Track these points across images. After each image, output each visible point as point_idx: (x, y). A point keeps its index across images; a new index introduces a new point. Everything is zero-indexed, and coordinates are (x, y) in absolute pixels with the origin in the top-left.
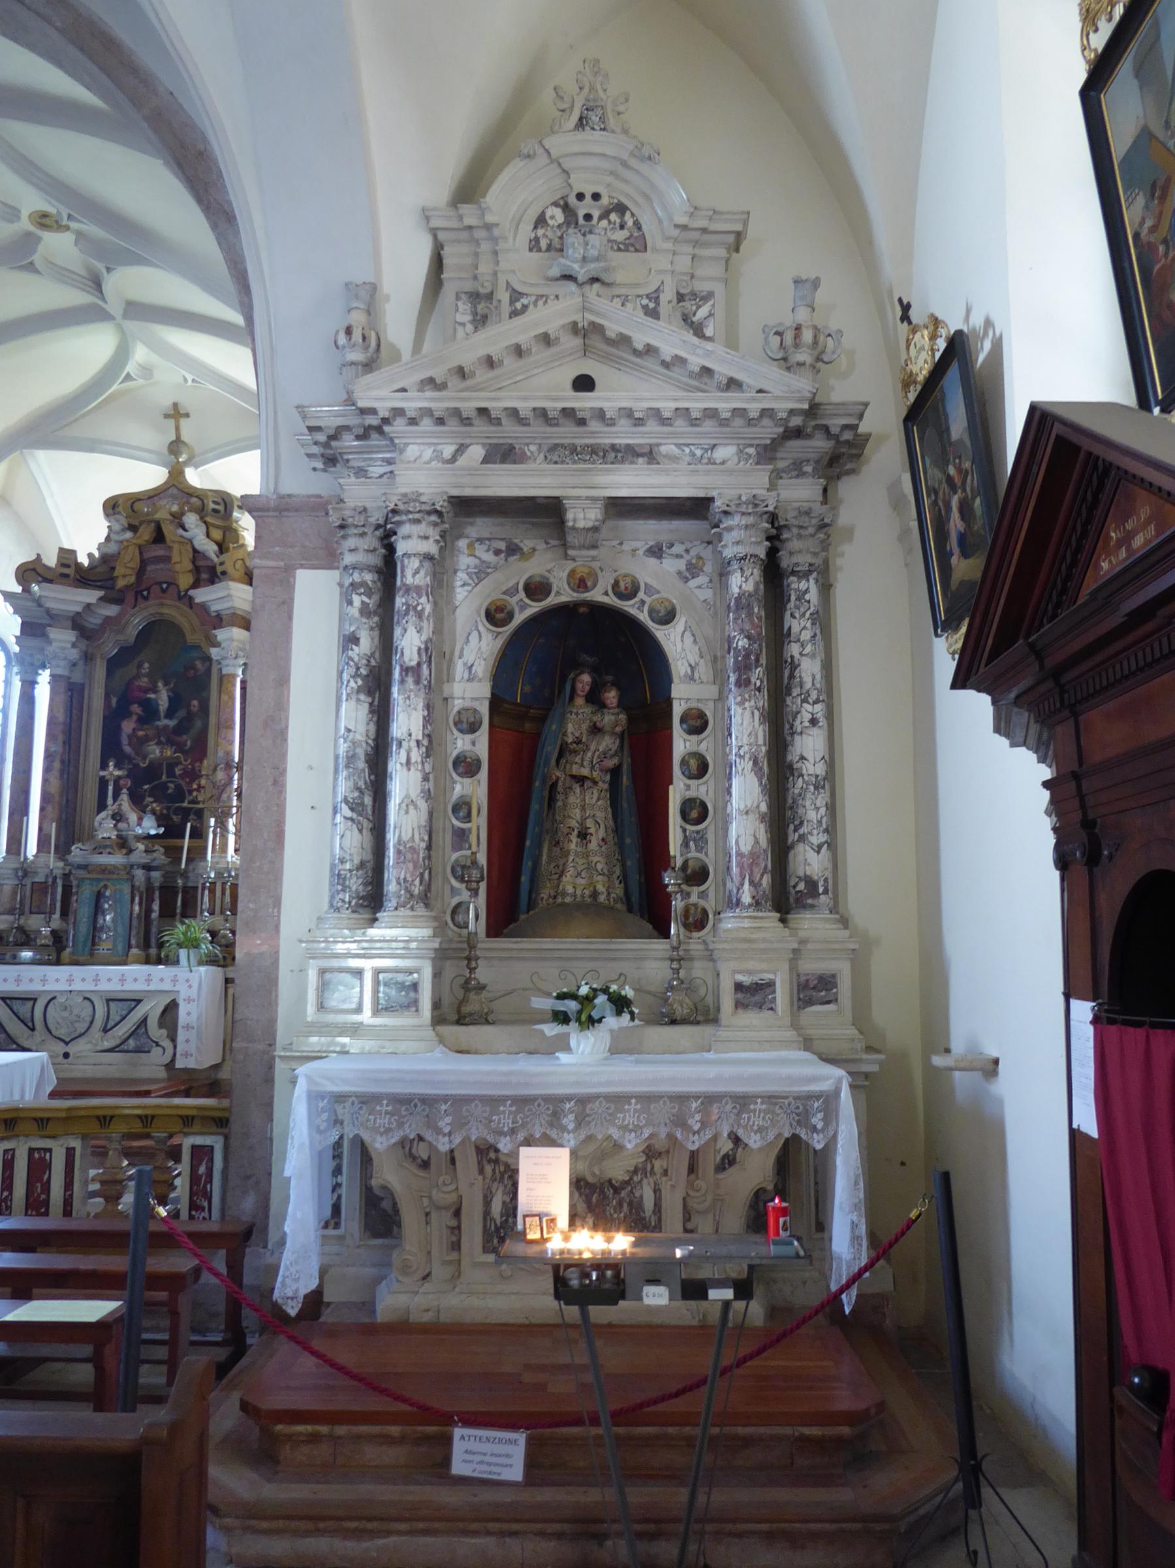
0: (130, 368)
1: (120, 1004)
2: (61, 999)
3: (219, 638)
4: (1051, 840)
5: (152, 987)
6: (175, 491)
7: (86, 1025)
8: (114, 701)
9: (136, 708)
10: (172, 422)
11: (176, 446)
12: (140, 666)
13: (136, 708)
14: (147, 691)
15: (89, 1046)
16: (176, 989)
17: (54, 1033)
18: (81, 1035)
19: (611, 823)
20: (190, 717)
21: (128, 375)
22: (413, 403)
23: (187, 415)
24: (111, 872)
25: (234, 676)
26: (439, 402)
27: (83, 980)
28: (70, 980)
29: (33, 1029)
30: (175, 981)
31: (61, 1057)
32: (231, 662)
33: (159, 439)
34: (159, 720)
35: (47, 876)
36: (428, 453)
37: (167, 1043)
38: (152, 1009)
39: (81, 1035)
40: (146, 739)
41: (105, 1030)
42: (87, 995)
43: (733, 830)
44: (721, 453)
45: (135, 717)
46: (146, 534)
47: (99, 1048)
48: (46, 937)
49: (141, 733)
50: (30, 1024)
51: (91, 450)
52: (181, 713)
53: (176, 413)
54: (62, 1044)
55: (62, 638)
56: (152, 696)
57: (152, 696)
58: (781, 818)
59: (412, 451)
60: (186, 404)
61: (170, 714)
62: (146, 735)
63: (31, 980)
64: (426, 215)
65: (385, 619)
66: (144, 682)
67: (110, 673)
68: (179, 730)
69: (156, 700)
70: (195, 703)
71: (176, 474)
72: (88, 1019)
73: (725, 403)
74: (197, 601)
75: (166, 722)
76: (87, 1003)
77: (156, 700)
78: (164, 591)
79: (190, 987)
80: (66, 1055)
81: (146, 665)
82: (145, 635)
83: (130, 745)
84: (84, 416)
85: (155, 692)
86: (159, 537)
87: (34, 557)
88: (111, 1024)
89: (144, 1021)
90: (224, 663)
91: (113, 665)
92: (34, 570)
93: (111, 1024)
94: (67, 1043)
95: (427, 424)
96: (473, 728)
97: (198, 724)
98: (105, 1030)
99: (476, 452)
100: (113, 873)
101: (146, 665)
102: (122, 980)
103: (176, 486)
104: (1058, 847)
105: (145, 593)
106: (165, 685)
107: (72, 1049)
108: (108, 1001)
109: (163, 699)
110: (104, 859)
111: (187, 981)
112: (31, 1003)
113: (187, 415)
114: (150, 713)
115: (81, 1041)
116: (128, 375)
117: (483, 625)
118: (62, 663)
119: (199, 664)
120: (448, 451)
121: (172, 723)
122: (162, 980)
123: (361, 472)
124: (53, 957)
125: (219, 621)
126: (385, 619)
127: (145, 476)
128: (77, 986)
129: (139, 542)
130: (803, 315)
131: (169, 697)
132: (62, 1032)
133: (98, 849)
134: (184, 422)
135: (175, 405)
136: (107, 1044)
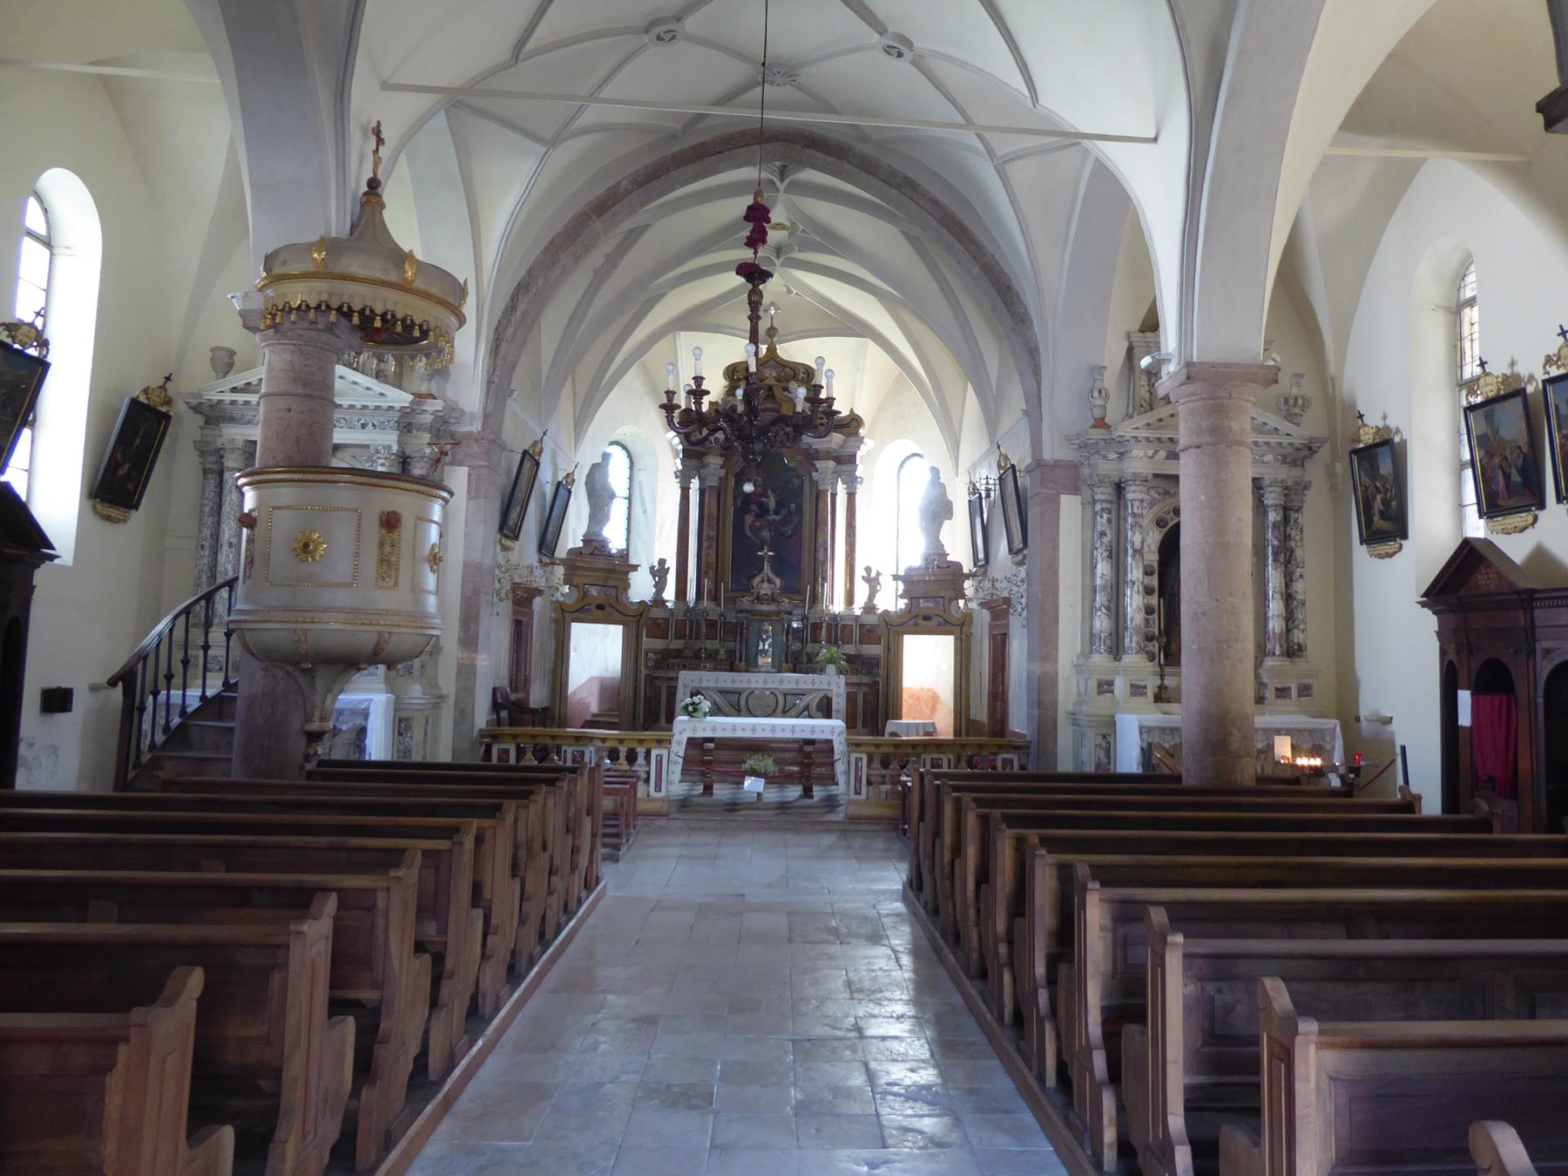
4: (1437, 644)
9: (754, 507)
13: (754, 507)
19: (820, 556)
20: (790, 514)
22: (1142, 434)
26: (1153, 434)
28: (765, 682)
36: (1142, 454)
40: (762, 528)
43: (1271, 626)
44: (1267, 458)
51: (716, 332)
52: (784, 512)
58: (1289, 617)
59: (1135, 452)
61: (776, 512)
64: (1128, 335)
65: (1118, 523)
68: (781, 523)
71: (772, 350)
73: (1273, 440)
95: (1144, 442)
96: (1152, 574)
97: (796, 519)
99: (1162, 454)
103: (772, 359)
104: (1441, 648)
108: (785, 695)
109: (772, 504)
110: (765, 608)
114: (763, 511)
117: (1155, 528)
120: (1150, 453)
121: (778, 518)
123: (1105, 457)
126: (1118, 523)
130: (1295, 391)
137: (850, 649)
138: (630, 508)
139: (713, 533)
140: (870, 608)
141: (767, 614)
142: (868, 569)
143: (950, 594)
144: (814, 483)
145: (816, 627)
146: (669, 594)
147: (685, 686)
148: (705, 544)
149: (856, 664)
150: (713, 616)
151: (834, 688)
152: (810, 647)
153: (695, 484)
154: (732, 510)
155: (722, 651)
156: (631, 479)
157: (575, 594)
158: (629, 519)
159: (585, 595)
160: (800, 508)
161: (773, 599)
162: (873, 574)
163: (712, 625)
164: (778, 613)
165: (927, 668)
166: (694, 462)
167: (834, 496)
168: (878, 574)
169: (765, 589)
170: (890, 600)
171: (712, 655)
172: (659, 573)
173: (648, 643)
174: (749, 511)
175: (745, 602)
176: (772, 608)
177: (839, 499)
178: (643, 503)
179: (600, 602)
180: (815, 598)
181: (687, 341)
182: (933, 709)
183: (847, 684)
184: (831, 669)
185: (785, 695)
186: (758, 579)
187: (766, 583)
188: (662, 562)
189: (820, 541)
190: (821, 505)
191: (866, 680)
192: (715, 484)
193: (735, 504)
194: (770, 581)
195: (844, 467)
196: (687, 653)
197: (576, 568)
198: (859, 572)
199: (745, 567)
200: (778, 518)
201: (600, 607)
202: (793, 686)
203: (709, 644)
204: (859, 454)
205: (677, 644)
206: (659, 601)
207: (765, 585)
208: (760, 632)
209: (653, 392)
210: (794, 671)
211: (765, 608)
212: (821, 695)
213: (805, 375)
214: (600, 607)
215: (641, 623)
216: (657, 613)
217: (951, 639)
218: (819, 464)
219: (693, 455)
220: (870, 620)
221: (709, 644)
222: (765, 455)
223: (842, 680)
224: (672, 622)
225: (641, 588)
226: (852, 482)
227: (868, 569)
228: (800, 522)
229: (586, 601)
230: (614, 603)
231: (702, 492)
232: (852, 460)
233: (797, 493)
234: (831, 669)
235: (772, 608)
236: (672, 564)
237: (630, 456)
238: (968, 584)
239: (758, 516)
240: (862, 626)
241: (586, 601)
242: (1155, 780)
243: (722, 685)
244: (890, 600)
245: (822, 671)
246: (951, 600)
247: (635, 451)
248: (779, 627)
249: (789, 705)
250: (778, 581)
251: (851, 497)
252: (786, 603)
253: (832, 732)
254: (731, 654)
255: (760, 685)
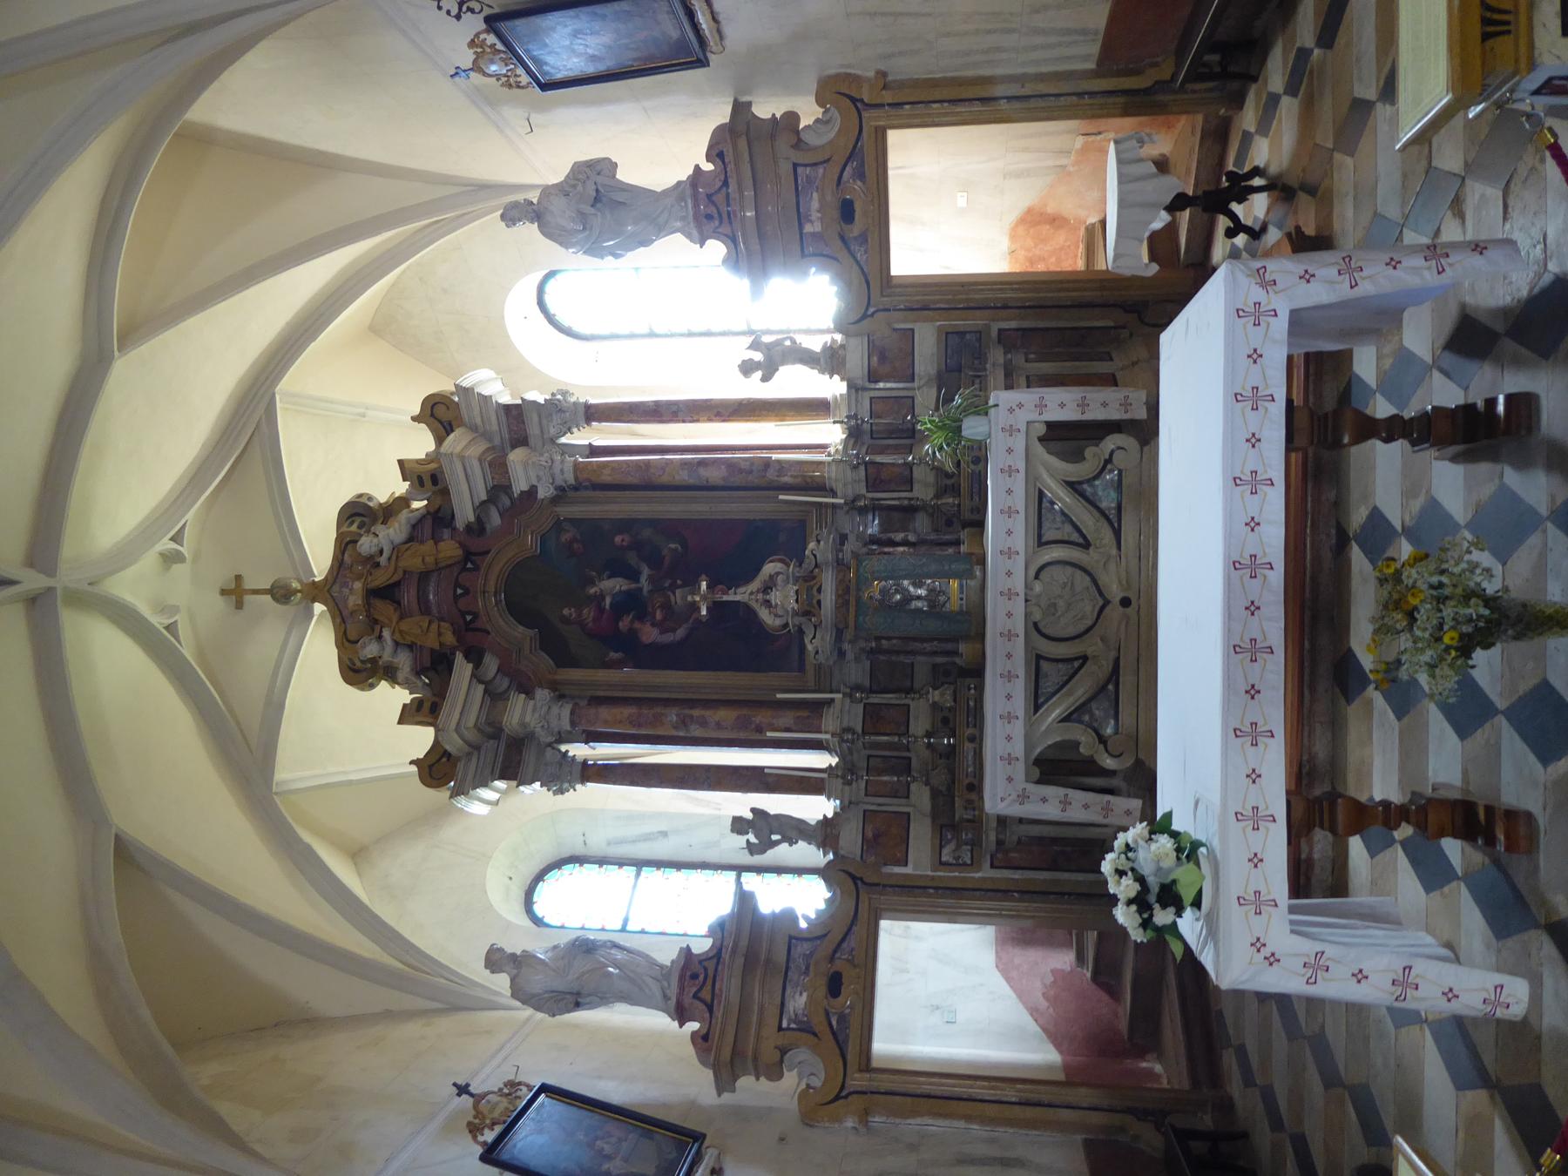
0: (158, 621)
1: (1046, 525)
2: (1037, 616)
3: (525, 487)
5: (1021, 465)
6: (336, 588)
7: (1079, 573)
8: (613, 655)
9: (624, 625)
10: (248, 598)
11: (281, 593)
12: (566, 621)
14: (601, 610)
15: (1112, 567)
16: (1023, 428)
17: (1089, 623)
18: (1095, 582)
21: (167, 628)
23: (238, 578)
24: (847, 590)
25: (576, 465)
27: (1009, 697)
29: (1085, 658)
30: (1011, 431)
31: (1128, 610)
32: (557, 470)
33: (270, 620)
34: (641, 589)
35: (853, 700)
37: (1111, 442)
38: (1054, 471)
39: (1095, 582)
40: (667, 607)
41: (1086, 545)
42: (1032, 573)
45: (637, 625)
46: (384, 609)
47: (1114, 552)
48: (942, 695)
49: (659, 615)
50: (1076, 664)
51: (281, 706)
53: (236, 593)
54: (1108, 610)
55: (520, 713)
56: (608, 600)
57: (608, 600)
60: (223, 577)
61: (633, 575)
62: (662, 607)
63: (1009, 615)
66: (588, 614)
67: (575, 663)
68: (655, 561)
69: (614, 596)
70: (618, 539)
71: (315, 591)
72: (1069, 570)
74: (472, 518)
75: (643, 579)
76: (1043, 575)
77: (614, 596)
78: (467, 592)
79: (1020, 406)
80: (1126, 602)
81: (566, 612)
82: (520, 611)
83: (674, 630)
84: (231, 711)
85: (602, 597)
86: (387, 593)
87: (414, 768)
88: (1075, 537)
89: (1073, 486)
90: (559, 482)
91: (564, 658)
92: (430, 767)
93: (1075, 537)
94: (1107, 603)
97: (647, 533)
98: (1086, 545)
100: (848, 588)
101: (566, 612)
102: (1010, 512)
105: (469, 618)
106: (593, 584)
107: (1115, 592)
108: (1041, 543)
109: (613, 586)
110: (828, 598)
111: (1011, 410)
112: (1045, 665)
113: (238, 578)
114: (631, 603)
115: (1103, 579)
116: (167, 628)
118: (555, 710)
119: (565, 537)
121: (646, 572)
122: (1010, 451)
124: (972, 683)
125: (499, 489)
127: (319, 645)
128: (1018, 583)
129: (395, 618)
131: (609, 577)
132: (1089, 608)
133: (809, 610)
134: (249, 584)
135: (224, 592)
136: (1107, 535)
137: (925, 397)
138: (659, 864)
139: (672, 715)
140: (830, 361)
141: (844, 592)
142: (747, 368)
143: (783, 144)
144: (562, 494)
145: (876, 478)
146: (815, 808)
147: (1023, 797)
148: (697, 732)
149: (964, 368)
150: (855, 717)
151: (1021, 418)
152: (923, 491)
153: (578, 750)
154: (628, 673)
155: (935, 696)
156: (602, 861)
157: (802, 1054)
158: (679, 865)
159: (806, 1028)
160: (626, 525)
161: (809, 580)
162: (758, 356)
163: (873, 716)
164: (841, 565)
165: (967, 208)
166: (529, 757)
167: (594, 451)
168: (755, 346)
169: (785, 597)
170: (810, 301)
171: (945, 721)
172: (764, 830)
173: (919, 861)
174: (633, 633)
175: (817, 644)
176: (828, 581)
177: (599, 442)
178: (647, 838)
179: (822, 991)
180: (808, 480)
181: (295, 766)
182: (1056, 221)
183: (1009, 387)
184: (973, 428)
185: (1041, 543)
186: (764, 615)
187: (773, 596)
188: (739, 825)
189: (684, 477)
190: (606, 478)
191: (997, 356)
192: (566, 711)
193: (617, 665)
194: (767, 588)
195: (533, 430)
196: (940, 778)
197: (736, 1053)
198: (754, 389)
199: (738, 643)
200: (646, 572)
201: (835, 985)
202: (1019, 524)
203: (920, 724)
204: (506, 399)
205: (921, 797)
206: (825, 833)
207: (775, 597)
208: (885, 605)
209: (434, 818)
210: (981, 524)
211: (828, 598)
212: (1039, 449)
213: (358, 514)
214: (835, 985)
215: (872, 884)
216: (851, 838)
217: (897, 140)
218: (520, 485)
219: (515, 759)
220: (857, 360)
221: (920, 724)
222: (545, 598)
223: (1001, 398)
224: (873, 804)
225: (799, 897)
226: (568, 412)
227: (747, 368)
228: (653, 523)
229: (819, 1023)
230: (827, 947)
231: (591, 737)
232: (515, 414)
233: (593, 531)
234: (973, 428)
235: (828, 581)
236: (742, 803)
237: (558, 864)
238: (766, 108)
239: (641, 617)
240: (873, 377)
241: (821, 1027)
242: (961, 612)
243: (1019, 705)
244: (810, 301)
245: (979, 454)
246: (798, 144)
247: (549, 853)
248: (873, 564)
249: (1067, 532)
250: (769, 568)
251: (594, 414)
252: (818, 548)
253: (1258, 315)
254: (941, 675)
255: (1019, 607)
